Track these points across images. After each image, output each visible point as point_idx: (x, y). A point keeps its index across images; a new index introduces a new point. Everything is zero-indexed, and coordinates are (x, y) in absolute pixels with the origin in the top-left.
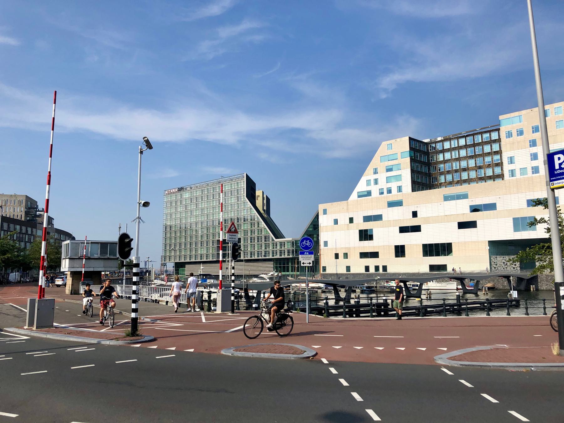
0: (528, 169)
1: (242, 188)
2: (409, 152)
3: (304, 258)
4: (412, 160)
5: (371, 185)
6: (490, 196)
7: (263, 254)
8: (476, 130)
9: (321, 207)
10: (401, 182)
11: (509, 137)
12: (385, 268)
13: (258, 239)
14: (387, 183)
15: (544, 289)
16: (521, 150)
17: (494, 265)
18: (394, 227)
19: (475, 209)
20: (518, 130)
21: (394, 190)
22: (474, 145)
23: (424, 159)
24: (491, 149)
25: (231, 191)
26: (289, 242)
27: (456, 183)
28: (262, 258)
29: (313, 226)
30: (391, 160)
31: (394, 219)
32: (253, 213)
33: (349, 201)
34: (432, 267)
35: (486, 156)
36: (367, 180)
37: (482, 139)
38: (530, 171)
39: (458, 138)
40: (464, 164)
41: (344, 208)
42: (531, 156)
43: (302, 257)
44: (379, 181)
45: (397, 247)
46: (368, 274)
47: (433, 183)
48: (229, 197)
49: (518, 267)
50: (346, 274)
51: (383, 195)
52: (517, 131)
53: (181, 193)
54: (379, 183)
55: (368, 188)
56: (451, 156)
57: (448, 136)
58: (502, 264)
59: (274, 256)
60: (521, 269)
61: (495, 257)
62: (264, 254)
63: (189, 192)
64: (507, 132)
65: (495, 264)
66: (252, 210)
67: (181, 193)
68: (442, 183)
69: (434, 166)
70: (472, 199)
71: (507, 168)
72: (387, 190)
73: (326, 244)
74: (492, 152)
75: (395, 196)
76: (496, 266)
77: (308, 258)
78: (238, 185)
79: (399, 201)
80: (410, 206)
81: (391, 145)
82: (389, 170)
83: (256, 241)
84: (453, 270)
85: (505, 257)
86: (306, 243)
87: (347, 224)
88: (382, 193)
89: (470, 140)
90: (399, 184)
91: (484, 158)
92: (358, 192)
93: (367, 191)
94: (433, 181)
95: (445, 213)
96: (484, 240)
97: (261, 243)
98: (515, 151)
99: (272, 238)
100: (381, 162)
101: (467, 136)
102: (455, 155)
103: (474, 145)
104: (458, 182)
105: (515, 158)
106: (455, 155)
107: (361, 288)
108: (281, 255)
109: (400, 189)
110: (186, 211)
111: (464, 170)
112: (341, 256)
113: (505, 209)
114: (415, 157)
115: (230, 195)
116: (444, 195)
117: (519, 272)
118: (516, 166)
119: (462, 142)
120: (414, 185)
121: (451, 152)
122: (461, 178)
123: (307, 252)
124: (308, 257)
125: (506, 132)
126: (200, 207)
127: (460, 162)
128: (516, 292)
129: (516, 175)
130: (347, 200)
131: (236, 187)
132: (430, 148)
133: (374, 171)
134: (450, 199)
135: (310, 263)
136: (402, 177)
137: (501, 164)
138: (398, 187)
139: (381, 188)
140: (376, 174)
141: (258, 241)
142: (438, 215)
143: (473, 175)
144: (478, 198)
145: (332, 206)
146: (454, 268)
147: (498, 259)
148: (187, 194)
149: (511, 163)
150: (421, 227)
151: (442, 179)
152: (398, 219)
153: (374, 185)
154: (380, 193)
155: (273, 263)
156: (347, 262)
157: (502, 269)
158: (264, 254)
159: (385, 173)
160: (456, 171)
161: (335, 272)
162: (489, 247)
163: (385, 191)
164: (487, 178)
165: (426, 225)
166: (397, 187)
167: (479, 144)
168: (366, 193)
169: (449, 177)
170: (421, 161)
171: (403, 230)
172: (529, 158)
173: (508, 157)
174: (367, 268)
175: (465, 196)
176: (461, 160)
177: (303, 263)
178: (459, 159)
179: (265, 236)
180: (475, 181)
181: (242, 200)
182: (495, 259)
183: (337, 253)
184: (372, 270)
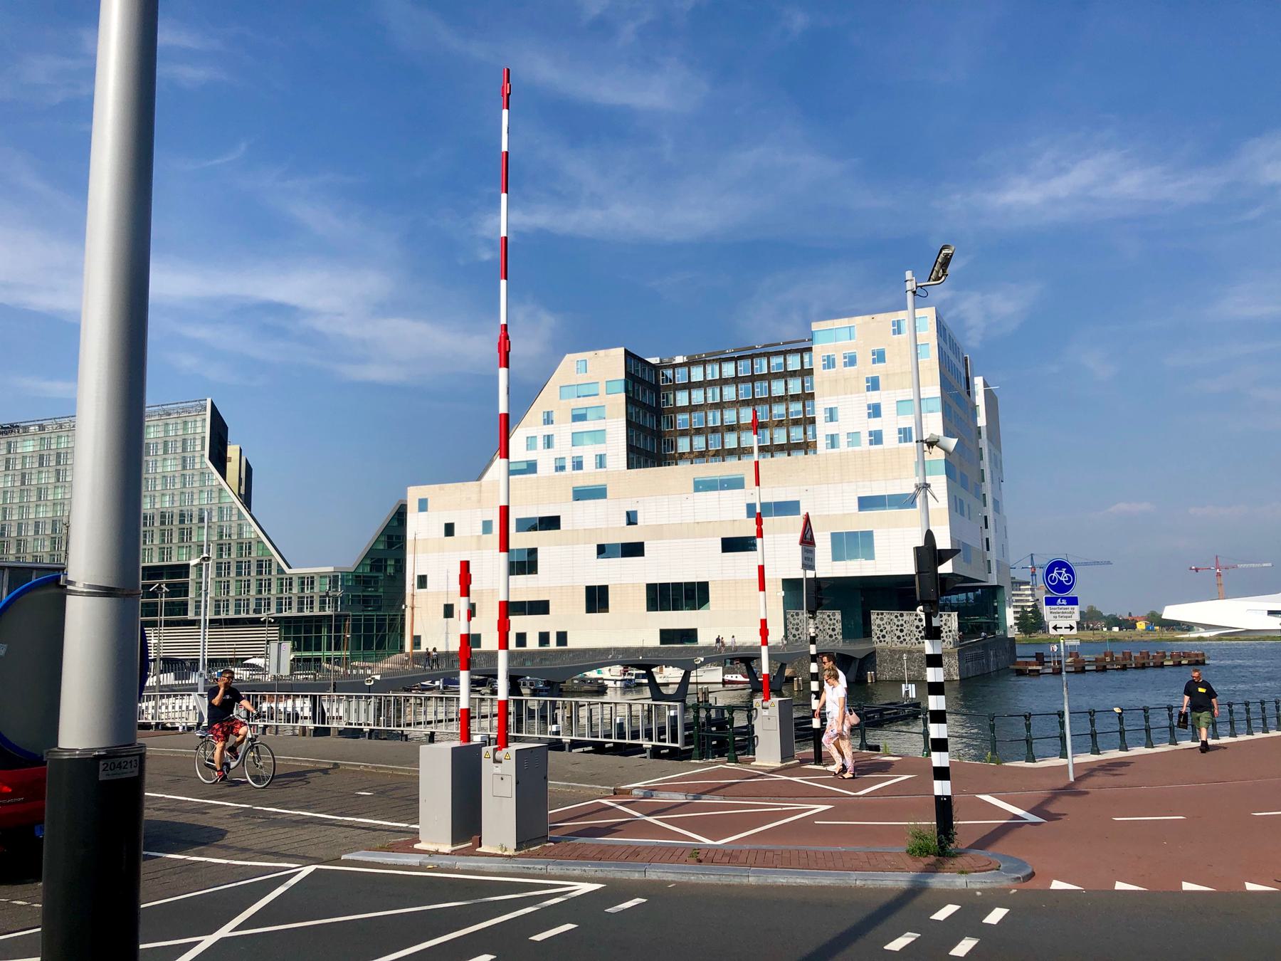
0: (862, 435)
1: (197, 437)
2: (623, 383)
3: (1057, 615)
4: (630, 401)
5: (535, 449)
6: (789, 486)
7: (252, 606)
8: (754, 348)
9: (413, 495)
10: (603, 445)
11: (829, 368)
12: (562, 638)
13: (239, 567)
14: (573, 446)
18: (585, 544)
22: (753, 379)
23: (648, 398)
24: (786, 389)
25: (166, 443)
26: (325, 577)
27: (714, 456)
28: (248, 616)
29: (386, 539)
30: (584, 396)
31: (586, 528)
32: (228, 500)
33: (483, 483)
34: (667, 636)
36: (527, 438)
37: (769, 367)
38: (865, 438)
40: (730, 416)
41: (470, 498)
43: (1051, 613)
44: (556, 440)
48: (159, 459)
51: (562, 473)
53: (9, 440)
54: (555, 444)
55: (530, 456)
56: (705, 398)
57: (698, 355)
58: (914, 629)
59: (282, 612)
61: (898, 615)
62: (254, 607)
63: (36, 438)
64: (826, 358)
66: (223, 494)
67: (9, 440)
68: (684, 453)
69: (668, 417)
71: (823, 429)
72: (573, 462)
73: (422, 581)
75: (589, 476)
76: (901, 634)
77: (1066, 615)
78: (185, 429)
81: (584, 362)
83: (233, 574)
84: (718, 640)
85: (882, 614)
86: (1060, 574)
88: (561, 468)
89: (744, 368)
90: (600, 449)
93: (527, 461)
95: (696, 517)
96: (774, 577)
97: (247, 578)
99: (278, 564)
100: (561, 398)
102: (713, 395)
103: (753, 379)
106: (713, 395)
107: (531, 684)
108: (301, 610)
109: (601, 461)
110: (23, 487)
111: (731, 428)
113: (817, 514)
114: (633, 395)
115: (161, 452)
116: (694, 479)
117: (841, 644)
119: (729, 370)
120: (631, 456)
122: (723, 446)
123: (1063, 598)
124: (1067, 611)
126: (34, 482)
127: (722, 411)
128: (914, 686)
130: (479, 478)
131: (180, 432)
132: (661, 378)
134: (726, 485)
135: (1071, 628)
136: (607, 436)
138: (598, 458)
139: (559, 457)
140: (548, 424)
141: (239, 574)
142: (680, 522)
145: (442, 492)
146: (720, 638)
147: (905, 618)
148: (27, 443)
151: (683, 445)
152: (594, 527)
153: (544, 448)
154: (556, 467)
155: (278, 628)
158: (254, 607)
160: (714, 430)
162: (783, 592)
163: (569, 465)
165: (655, 542)
167: (762, 378)
168: (524, 466)
169: (699, 443)
170: (645, 404)
172: (866, 411)
175: (737, 484)
176: (724, 407)
177: (1055, 628)
178: (721, 406)
179: (258, 561)
181: (198, 466)
182: (899, 617)
183: (450, 603)
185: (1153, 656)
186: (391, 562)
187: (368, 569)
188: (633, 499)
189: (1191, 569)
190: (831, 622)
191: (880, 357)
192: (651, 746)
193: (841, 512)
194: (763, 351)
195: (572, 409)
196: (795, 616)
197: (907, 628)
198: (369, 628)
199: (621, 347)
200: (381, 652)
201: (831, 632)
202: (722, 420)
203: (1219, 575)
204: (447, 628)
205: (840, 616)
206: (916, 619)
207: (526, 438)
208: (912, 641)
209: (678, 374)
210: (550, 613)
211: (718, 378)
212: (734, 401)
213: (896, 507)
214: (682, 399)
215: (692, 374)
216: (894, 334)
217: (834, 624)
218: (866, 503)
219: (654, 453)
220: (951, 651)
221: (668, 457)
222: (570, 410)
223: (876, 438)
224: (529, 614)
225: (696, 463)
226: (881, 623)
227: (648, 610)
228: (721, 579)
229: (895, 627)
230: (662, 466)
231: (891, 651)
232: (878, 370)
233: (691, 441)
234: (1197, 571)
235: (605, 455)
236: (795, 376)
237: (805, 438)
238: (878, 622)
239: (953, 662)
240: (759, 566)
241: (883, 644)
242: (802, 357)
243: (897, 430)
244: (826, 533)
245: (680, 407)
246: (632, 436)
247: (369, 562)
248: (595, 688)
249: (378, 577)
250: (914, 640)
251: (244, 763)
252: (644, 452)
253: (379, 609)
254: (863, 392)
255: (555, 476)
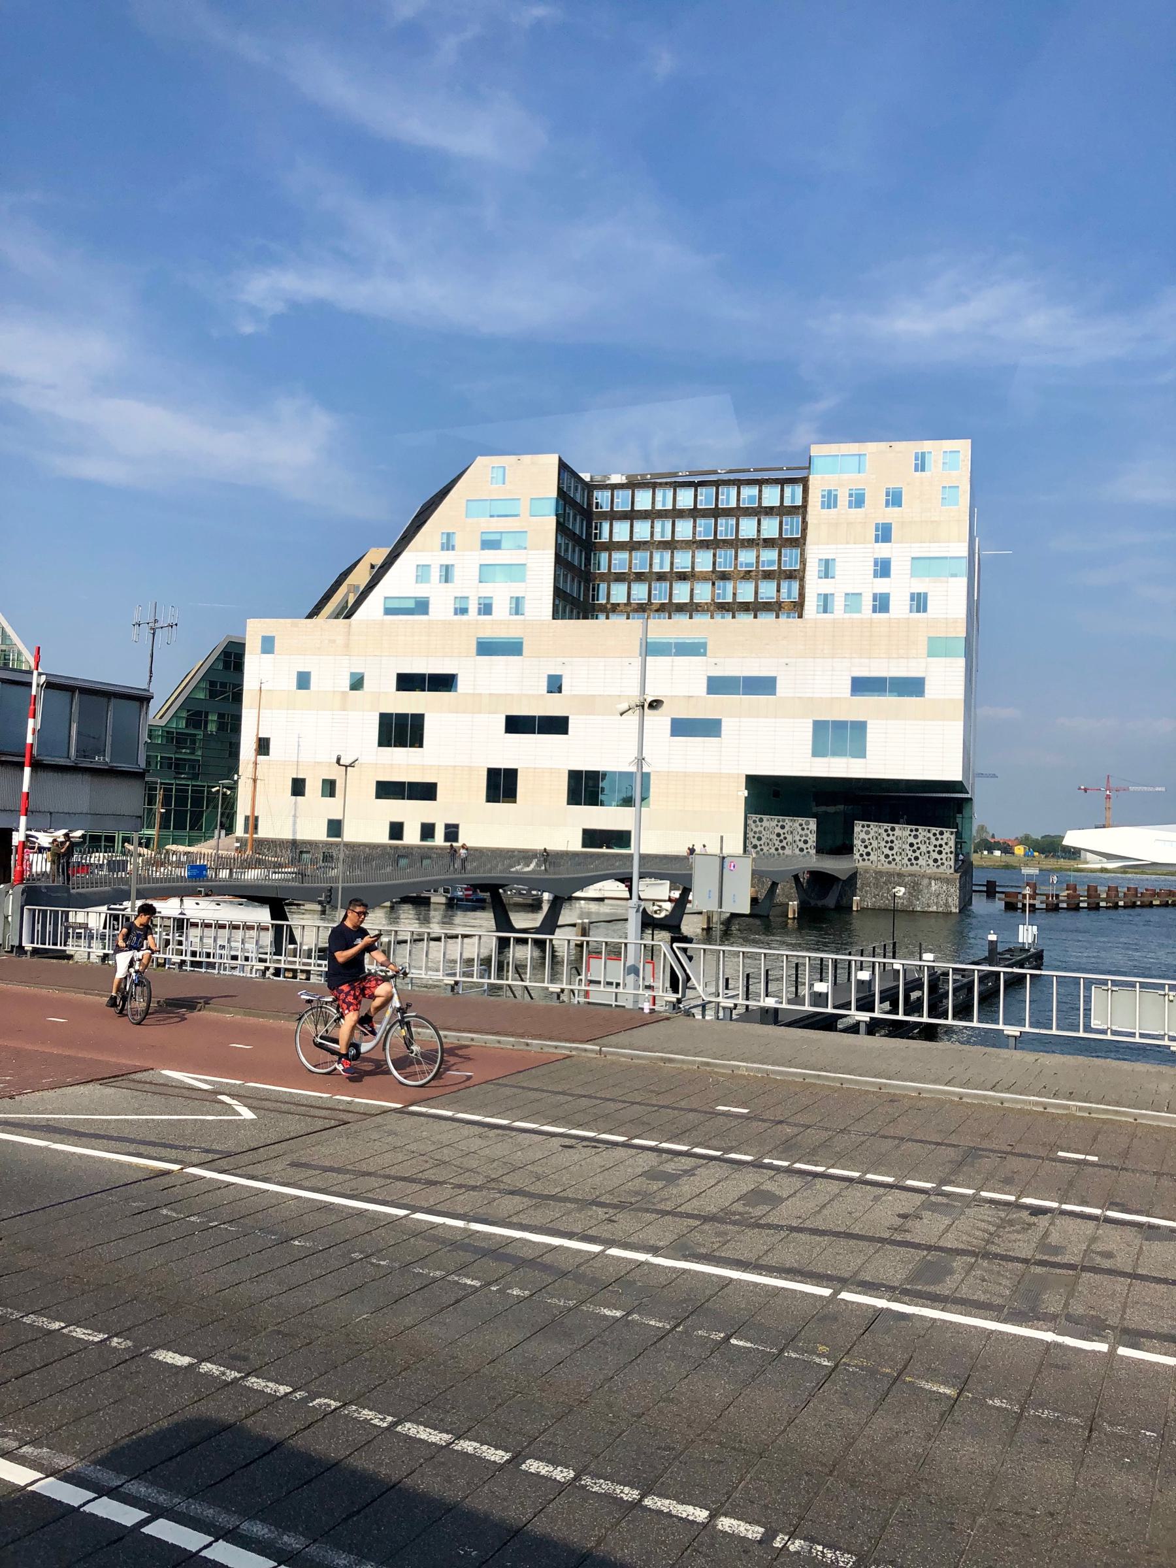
9: (254, 631)
10: (523, 585)
11: (829, 507)
12: (452, 832)
14: (480, 582)
15: (868, 905)
16: (854, 546)
17: (752, 840)
19: (717, 685)
20: (854, 492)
21: (501, 609)
22: (716, 513)
24: (759, 531)
27: (657, 611)
29: (208, 687)
30: (498, 516)
34: (592, 837)
35: (743, 546)
37: (738, 500)
38: (867, 603)
39: (676, 485)
40: (683, 561)
41: (334, 641)
42: (876, 564)
44: (457, 573)
45: (493, 774)
46: (396, 847)
47: (593, 600)
49: (812, 848)
50: (327, 844)
51: (464, 618)
52: (851, 495)
54: (455, 578)
55: (421, 591)
58: (907, 847)
60: (818, 852)
61: (757, 820)
64: (826, 493)
65: (756, 836)
70: (716, 660)
71: (814, 585)
72: (480, 604)
73: (263, 746)
74: (759, 539)
75: (500, 625)
76: (890, 853)
79: (494, 640)
80: (545, 659)
81: (502, 469)
82: (490, 544)
87: (343, 692)
89: (706, 500)
90: (517, 589)
91: (736, 553)
92: (386, 598)
93: (415, 598)
94: (593, 595)
98: (839, 546)
101: (702, 484)
102: (663, 530)
103: (716, 513)
104: (662, 608)
105: (837, 564)
106: (663, 530)
109: (517, 606)
111: (683, 577)
112: (313, 787)
118: (836, 587)
119: (685, 498)
121: (653, 523)
125: (822, 490)
129: (833, 609)
133: (445, 541)
136: (528, 573)
137: (777, 576)
140: (448, 549)
143: (703, 593)
144: (733, 657)
147: (765, 823)
149: (826, 576)
150: (570, 721)
153: (440, 582)
154: (456, 609)
156: (332, 808)
157: (773, 851)
159: (477, 553)
160: (661, 577)
161: (287, 835)
162: (746, 792)
163: (473, 608)
164: (738, 606)
165: (584, 717)
166: (512, 598)
167: (728, 513)
168: (411, 604)
169: (640, 592)
171: (516, 725)
172: (870, 568)
173: (820, 560)
174: (396, 830)
175: (695, 649)
176: (676, 548)
178: (671, 545)
180: (708, 611)
184: (412, 836)
185: (1142, 893)
186: (213, 717)
187: (183, 724)
188: (558, 659)
189: (1080, 789)
190: (803, 833)
191: (895, 499)
192: (868, 1019)
193: (829, 696)
194: (732, 477)
195: (482, 533)
196: (758, 822)
197: (898, 845)
198: (182, 801)
199: (554, 453)
200: (195, 833)
201: (801, 845)
202: (672, 564)
203: (1108, 797)
204: (295, 810)
205: (815, 826)
206: (910, 835)
207: (415, 567)
208: (900, 858)
209: (618, 498)
210: (438, 799)
211: (671, 508)
212: (690, 541)
213: (896, 694)
214: (621, 532)
215: (636, 500)
216: (916, 470)
217: (807, 835)
218: (861, 686)
219: (579, 600)
220: (951, 876)
221: (597, 608)
222: (479, 534)
223: (882, 603)
224: (410, 798)
225: (633, 618)
226: (866, 837)
227: (568, 804)
228: (667, 770)
229: (883, 844)
230: (588, 619)
231: (876, 873)
232: (891, 515)
233: (629, 588)
234: (1086, 792)
235: (523, 597)
236: (772, 515)
237: (778, 596)
238: (863, 835)
239: (952, 890)
240: (267, 754)
241: (867, 863)
242: (782, 491)
243: (909, 595)
244: (665, 718)
245: (618, 542)
246: (559, 575)
247: (184, 714)
248: (530, 902)
249: (195, 735)
250: (906, 861)
251: (384, 1045)
252: (571, 598)
253: (195, 777)
254: (870, 543)
255: (453, 620)
